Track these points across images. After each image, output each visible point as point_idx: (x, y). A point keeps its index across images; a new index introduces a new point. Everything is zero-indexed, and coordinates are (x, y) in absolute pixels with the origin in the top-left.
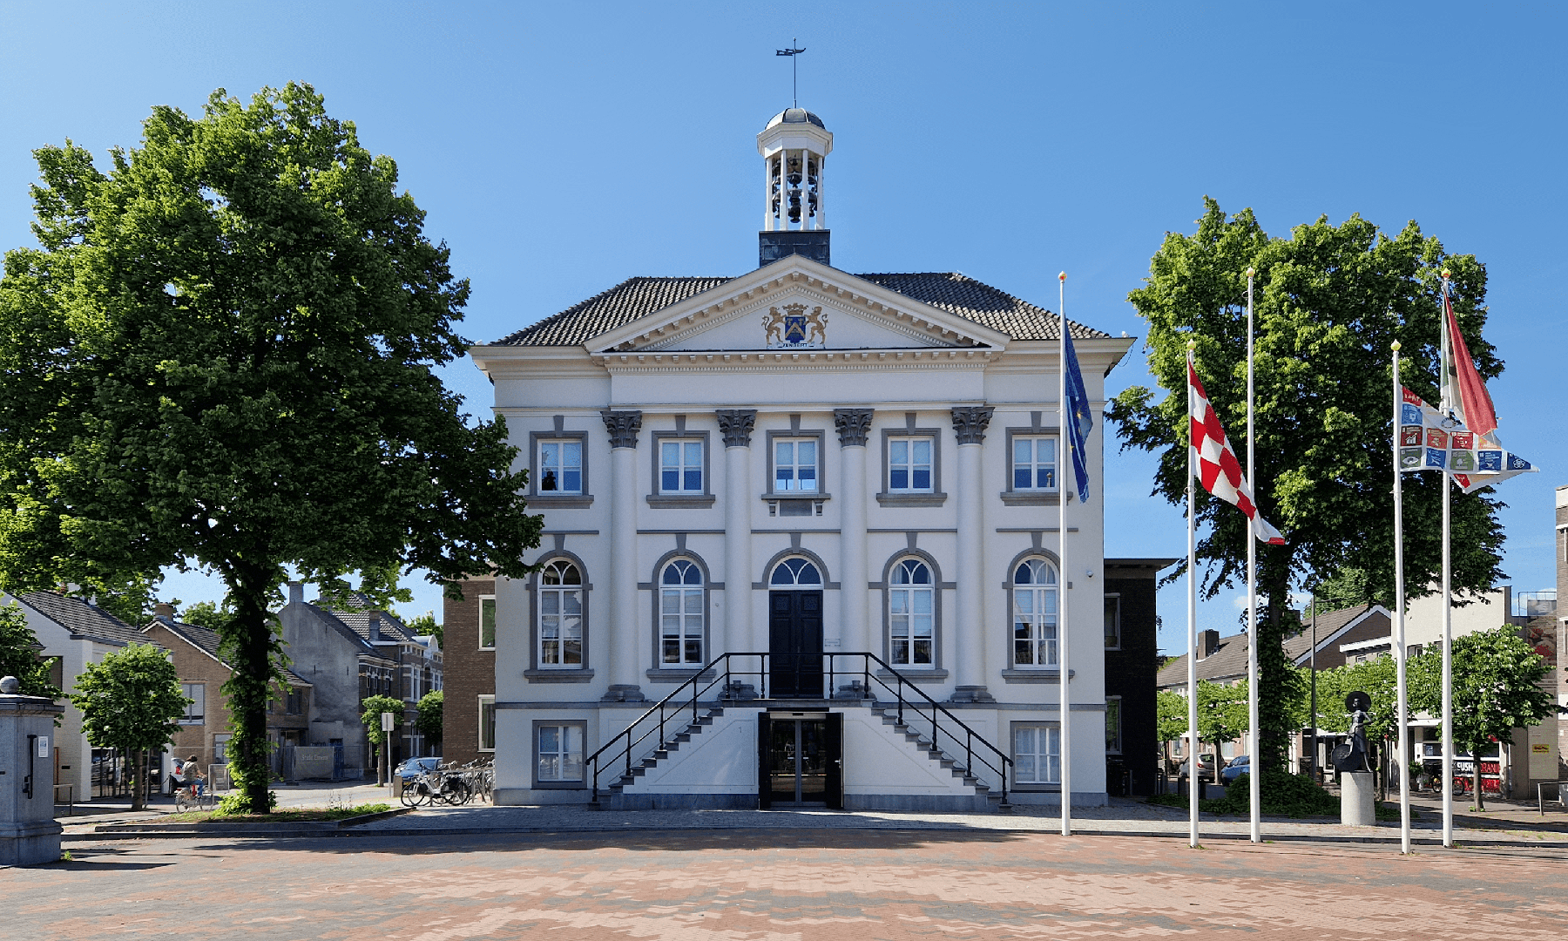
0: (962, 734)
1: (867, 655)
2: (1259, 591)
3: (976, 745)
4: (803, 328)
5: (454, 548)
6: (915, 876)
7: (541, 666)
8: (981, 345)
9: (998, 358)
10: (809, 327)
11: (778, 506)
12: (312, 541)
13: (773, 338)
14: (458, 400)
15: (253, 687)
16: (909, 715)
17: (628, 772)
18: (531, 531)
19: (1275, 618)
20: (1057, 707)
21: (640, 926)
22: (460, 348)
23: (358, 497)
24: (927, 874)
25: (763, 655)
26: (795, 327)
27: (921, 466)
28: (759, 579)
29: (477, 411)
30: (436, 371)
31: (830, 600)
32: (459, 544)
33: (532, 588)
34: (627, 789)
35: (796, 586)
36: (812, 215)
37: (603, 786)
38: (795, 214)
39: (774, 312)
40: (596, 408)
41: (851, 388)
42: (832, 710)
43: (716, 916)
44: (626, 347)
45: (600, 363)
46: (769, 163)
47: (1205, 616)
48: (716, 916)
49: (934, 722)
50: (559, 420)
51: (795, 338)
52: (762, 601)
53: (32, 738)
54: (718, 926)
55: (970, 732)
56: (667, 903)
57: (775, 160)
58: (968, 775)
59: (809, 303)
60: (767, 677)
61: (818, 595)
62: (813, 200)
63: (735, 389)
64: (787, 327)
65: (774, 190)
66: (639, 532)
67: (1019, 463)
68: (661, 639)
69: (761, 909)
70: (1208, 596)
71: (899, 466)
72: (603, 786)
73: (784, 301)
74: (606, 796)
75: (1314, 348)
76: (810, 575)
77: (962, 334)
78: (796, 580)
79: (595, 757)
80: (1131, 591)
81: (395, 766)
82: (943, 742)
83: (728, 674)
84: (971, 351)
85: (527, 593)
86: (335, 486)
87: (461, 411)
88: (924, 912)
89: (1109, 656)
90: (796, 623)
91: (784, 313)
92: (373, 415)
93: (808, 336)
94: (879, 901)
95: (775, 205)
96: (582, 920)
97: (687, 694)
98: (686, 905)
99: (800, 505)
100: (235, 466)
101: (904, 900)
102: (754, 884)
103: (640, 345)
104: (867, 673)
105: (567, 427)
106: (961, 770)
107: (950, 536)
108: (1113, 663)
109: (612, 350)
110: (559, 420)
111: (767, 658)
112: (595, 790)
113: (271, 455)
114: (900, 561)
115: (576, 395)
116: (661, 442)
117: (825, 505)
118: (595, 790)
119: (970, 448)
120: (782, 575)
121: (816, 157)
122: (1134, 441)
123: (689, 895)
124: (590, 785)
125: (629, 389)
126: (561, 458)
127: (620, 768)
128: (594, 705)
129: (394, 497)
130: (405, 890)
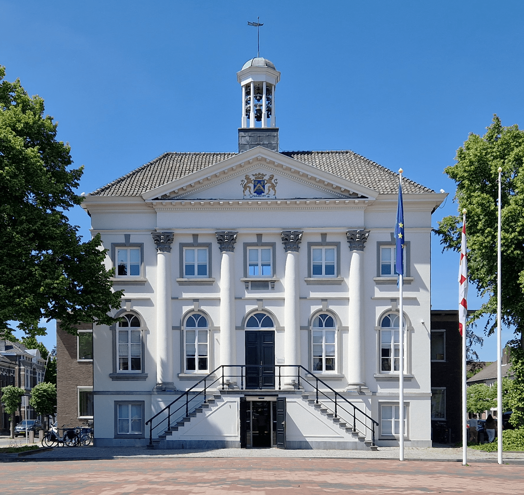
3: (358, 414)
4: (264, 187)
5: (74, 309)
6: (319, 475)
7: (118, 371)
8: (363, 197)
9: (371, 204)
10: (266, 186)
11: (250, 284)
13: (247, 192)
14: (76, 228)
17: (169, 429)
18: (115, 300)
21: (195, 489)
22: (78, 200)
23: (27, 284)
24: (324, 474)
25: (242, 366)
26: (259, 186)
27: (330, 263)
28: (239, 325)
29: (85, 236)
30: (65, 213)
32: (78, 307)
33: (113, 329)
34: (168, 438)
36: (268, 117)
37: (155, 436)
38: (258, 118)
39: (247, 178)
40: (148, 230)
41: (291, 220)
42: (280, 396)
43: (228, 486)
45: (151, 206)
46: (244, 89)
48: (228, 486)
49: (336, 402)
50: (127, 237)
51: (259, 192)
54: (229, 489)
55: (355, 408)
56: (205, 483)
57: (248, 86)
59: (267, 173)
60: (244, 378)
62: (269, 110)
63: (225, 220)
65: (247, 103)
66: (173, 298)
67: (384, 261)
68: (185, 357)
69: (249, 484)
71: (317, 262)
72: (155, 436)
73: (252, 172)
74: (157, 442)
76: (269, 322)
77: (352, 191)
78: (260, 325)
79: (151, 421)
81: (15, 425)
82: (340, 413)
83: (223, 376)
84: (357, 200)
85: (110, 333)
86: (15, 277)
88: (319, 486)
89: (433, 365)
90: (258, 350)
91: (253, 178)
92: (32, 240)
93: (266, 191)
94: (299, 483)
95: (248, 111)
96: (169, 488)
98: (213, 483)
101: (311, 483)
103: (172, 196)
105: (132, 240)
109: (157, 199)
110: (127, 237)
111: (244, 368)
112: (151, 438)
114: (318, 315)
115: (139, 225)
116: (184, 248)
118: (151, 438)
120: (252, 322)
122: (450, 246)
123: (214, 481)
124: (147, 435)
125: (167, 219)
126: (128, 257)
127: (164, 427)
128: (150, 393)
129: (47, 284)
130: (79, 479)
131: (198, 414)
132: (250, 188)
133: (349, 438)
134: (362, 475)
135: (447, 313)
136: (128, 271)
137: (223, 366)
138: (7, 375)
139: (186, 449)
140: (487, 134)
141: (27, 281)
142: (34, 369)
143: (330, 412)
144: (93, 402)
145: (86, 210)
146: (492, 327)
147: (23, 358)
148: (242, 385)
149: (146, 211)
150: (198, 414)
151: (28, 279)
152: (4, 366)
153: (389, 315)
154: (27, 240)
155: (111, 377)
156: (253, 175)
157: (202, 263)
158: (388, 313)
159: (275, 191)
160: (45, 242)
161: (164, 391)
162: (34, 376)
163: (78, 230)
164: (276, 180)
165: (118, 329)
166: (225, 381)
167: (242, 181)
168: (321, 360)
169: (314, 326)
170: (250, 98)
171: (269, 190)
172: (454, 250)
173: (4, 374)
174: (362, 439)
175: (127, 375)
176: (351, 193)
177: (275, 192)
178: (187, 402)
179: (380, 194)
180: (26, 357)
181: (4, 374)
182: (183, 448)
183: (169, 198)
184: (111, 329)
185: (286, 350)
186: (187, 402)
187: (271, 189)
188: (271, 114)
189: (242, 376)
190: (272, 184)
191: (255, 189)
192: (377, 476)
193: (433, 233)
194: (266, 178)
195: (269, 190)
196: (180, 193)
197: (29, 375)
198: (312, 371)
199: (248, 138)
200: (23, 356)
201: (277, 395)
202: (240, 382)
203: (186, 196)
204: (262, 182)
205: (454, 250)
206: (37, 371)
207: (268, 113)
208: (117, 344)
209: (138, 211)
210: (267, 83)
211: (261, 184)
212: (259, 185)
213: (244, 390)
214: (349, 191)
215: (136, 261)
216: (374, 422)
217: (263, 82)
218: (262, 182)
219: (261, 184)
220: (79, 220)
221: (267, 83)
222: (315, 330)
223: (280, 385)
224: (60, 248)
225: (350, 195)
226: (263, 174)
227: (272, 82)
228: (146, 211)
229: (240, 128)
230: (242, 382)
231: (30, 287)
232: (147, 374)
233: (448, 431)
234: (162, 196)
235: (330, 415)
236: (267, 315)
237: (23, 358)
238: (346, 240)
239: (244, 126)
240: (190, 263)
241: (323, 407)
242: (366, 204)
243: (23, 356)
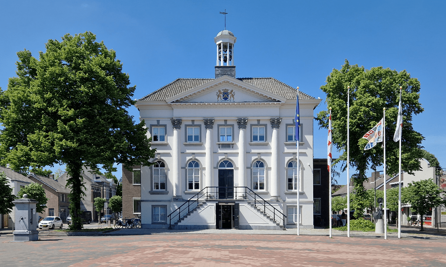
2: (358, 169)
4: (228, 96)
7: (154, 190)
8: (278, 101)
10: (229, 96)
12: (95, 157)
13: (219, 98)
14: (132, 117)
15: (77, 196)
18: (152, 154)
19: (361, 177)
20: (296, 203)
22: (133, 103)
23: (107, 145)
25: (217, 187)
26: (226, 95)
27: (262, 135)
28: (215, 166)
29: (137, 121)
32: (133, 157)
33: (151, 168)
36: (230, 60)
37: (172, 223)
38: (225, 61)
39: (219, 91)
40: (168, 118)
41: (242, 113)
44: (177, 101)
45: (170, 105)
46: (218, 46)
47: (343, 176)
50: (158, 121)
51: (226, 99)
53: (32, 209)
55: (275, 208)
57: (220, 45)
58: (274, 221)
59: (229, 89)
62: (231, 57)
63: (208, 113)
65: (220, 53)
70: (343, 171)
71: (255, 134)
73: (222, 88)
74: (173, 226)
75: (370, 104)
76: (230, 165)
79: (170, 215)
80: (320, 168)
81: (101, 217)
84: (275, 103)
85: (150, 170)
87: (133, 120)
90: (225, 179)
91: (222, 91)
92: (110, 123)
93: (229, 98)
95: (220, 58)
100: (75, 137)
101: (252, 247)
102: (217, 244)
103: (181, 100)
108: (315, 188)
109: (173, 102)
110: (158, 121)
113: (84, 133)
115: (164, 115)
116: (187, 127)
121: (232, 44)
122: (323, 126)
123: (202, 246)
125: (178, 113)
126: (159, 132)
127: (177, 218)
128: (170, 201)
132: (221, 96)
133: (271, 224)
136: (159, 139)
137: (207, 187)
150: (194, 212)
168: (257, 184)
169: (254, 167)
174: (278, 224)
185: (239, 179)
193: (314, 119)
194: (229, 91)
196: (185, 99)
198: (253, 190)
199: (220, 71)
206: (112, 190)
210: (229, 43)
216: (284, 216)
220: (134, 113)
221: (229, 43)
222: (254, 169)
227: (232, 42)
235: (262, 212)
236: (230, 161)
240: (191, 135)
241: (258, 208)
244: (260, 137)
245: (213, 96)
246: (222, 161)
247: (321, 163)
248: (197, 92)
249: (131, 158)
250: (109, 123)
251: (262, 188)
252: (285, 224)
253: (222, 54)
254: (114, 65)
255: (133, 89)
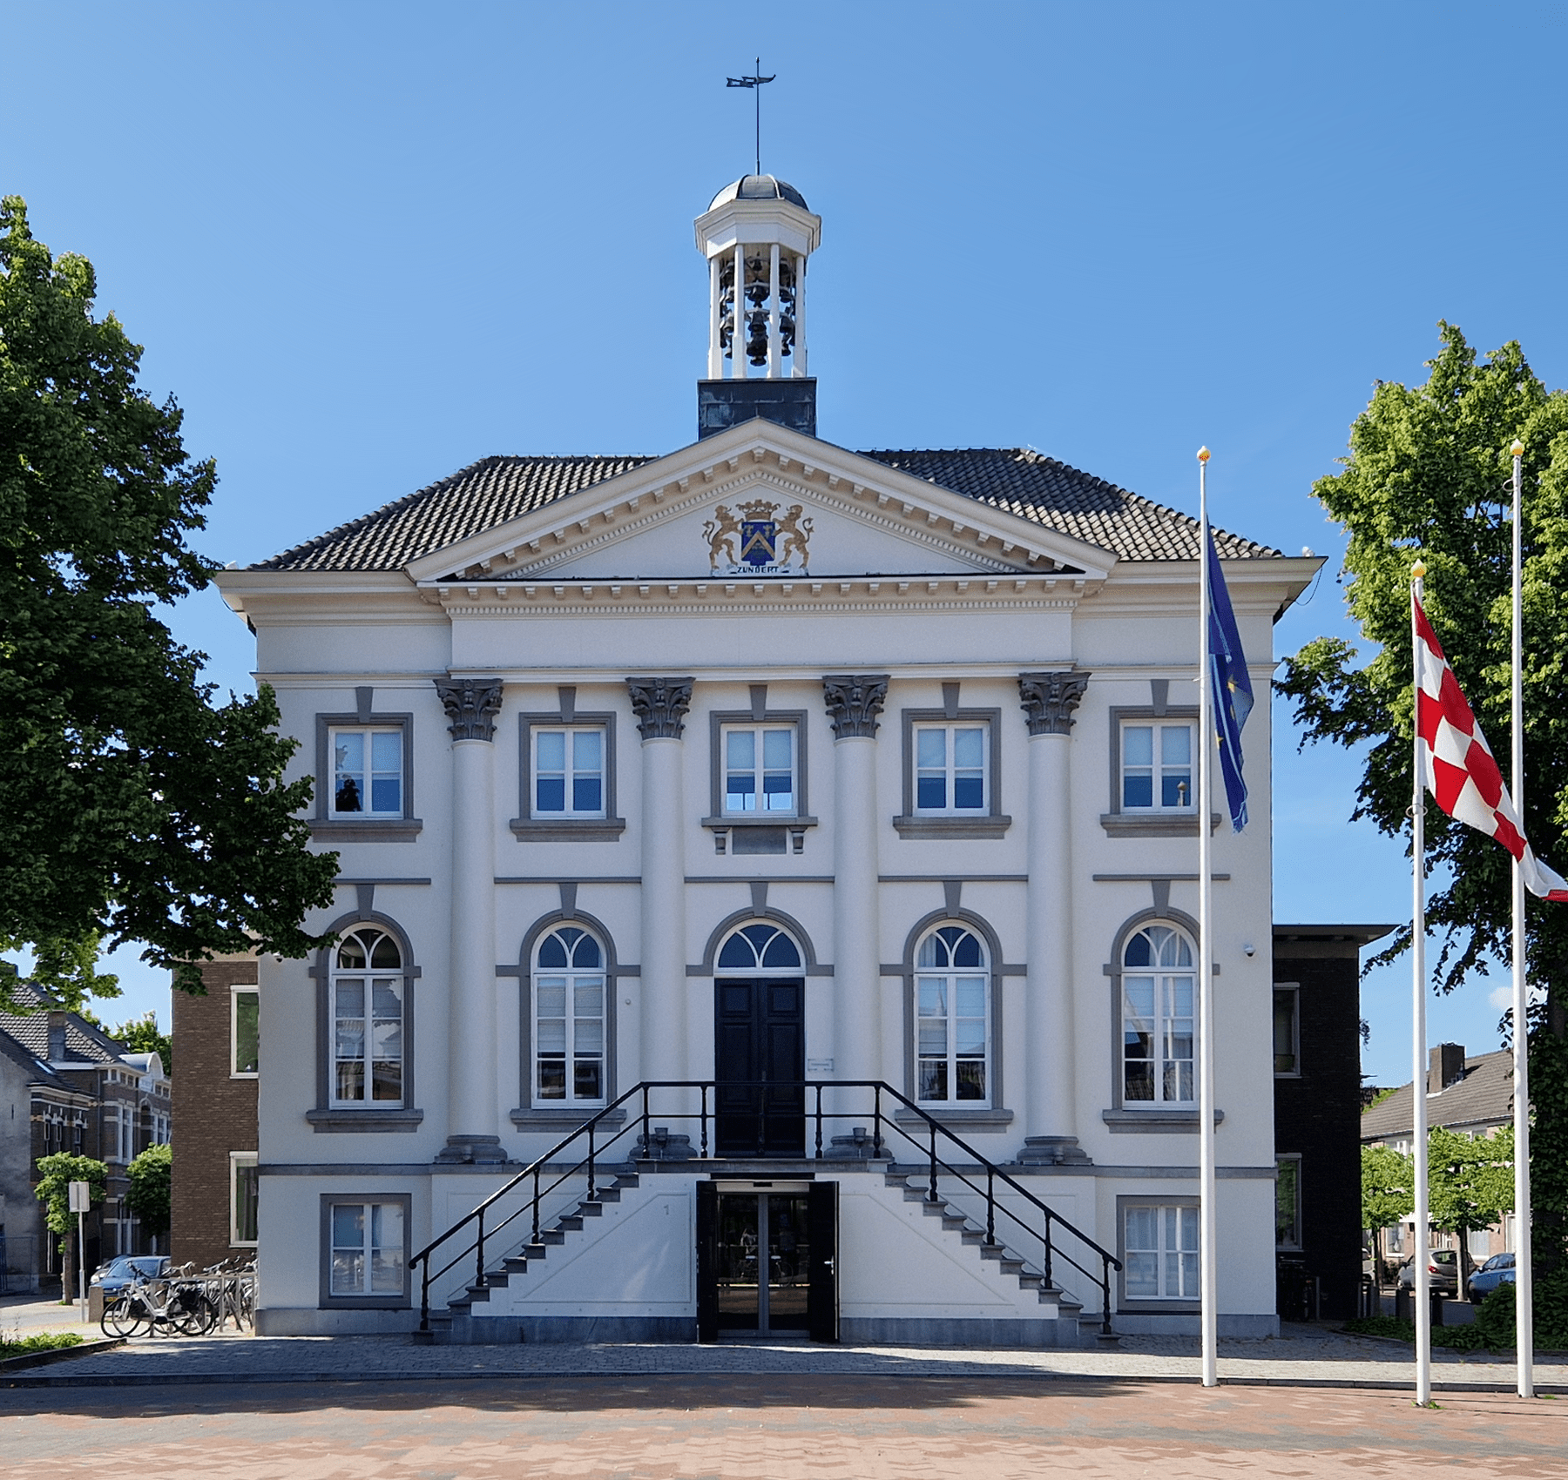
0: (1036, 1218)
1: (878, 1085)
2: (1531, 979)
3: (1059, 1234)
4: (771, 541)
5: (190, 908)
8: (1068, 570)
9: (1095, 590)
10: (780, 540)
11: (729, 837)
13: (722, 554)
16: (948, 1186)
17: (480, 1282)
18: (318, 879)
20: (1193, 1172)
22: (200, 574)
23: (31, 821)
25: (704, 1085)
28: (697, 959)
29: (227, 680)
30: (160, 612)
31: (816, 994)
32: (198, 900)
34: (478, 1309)
35: (759, 971)
36: (786, 353)
37: (438, 1302)
38: (757, 351)
39: (722, 515)
45: (432, 599)
49: (990, 1197)
50: (364, 695)
51: (758, 557)
52: (703, 994)
55: (1049, 1214)
57: (725, 261)
60: (711, 1122)
61: (797, 985)
62: (788, 328)
64: (745, 540)
67: (1131, 766)
68: (535, 1060)
70: (1447, 987)
71: (932, 770)
73: (738, 496)
74: (443, 1320)
76: (783, 953)
77: (1036, 552)
78: (759, 962)
79: (424, 1255)
80: (1317, 979)
81: (90, 1271)
82: (1005, 1230)
83: (646, 1117)
84: (1051, 579)
85: (310, 985)
87: (201, 679)
90: (760, 1033)
91: (739, 515)
92: (55, 685)
93: (779, 554)
97: (578, 1150)
99: (765, 835)
103: (499, 569)
104: (877, 1116)
105: (379, 706)
106: (1036, 1278)
107: (629, 891)
109: (452, 578)
110: (364, 695)
111: (711, 1091)
112: (425, 1310)
114: (932, 929)
115: (389, 651)
116: (534, 730)
117: (809, 835)
118: (425, 1310)
119: (1050, 742)
120: (736, 953)
122: (1322, 730)
125: (482, 642)
126: (367, 758)
127: (466, 1274)
131: (569, 1235)
132: (730, 544)
134: (1107, 1451)
135: (1313, 933)
136: (367, 798)
138: (66, 1123)
139: (532, 1342)
140: (1430, 382)
141: (29, 814)
142: (146, 1108)
143: (972, 1227)
144: (256, 1198)
145: (244, 616)
146: (1457, 966)
147: (114, 1077)
148: (704, 1144)
149: (415, 616)
150: (569, 1235)
151: (34, 809)
152: (55, 1099)
153: (1147, 931)
154: (37, 685)
155: (310, 1121)
156: (741, 507)
157: (587, 771)
158: (1145, 925)
159: (806, 554)
160: (94, 690)
161: (471, 1162)
162: (146, 1127)
163: (202, 667)
164: (810, 520)
165: (335, 972)
166: (651, 1131)
167: (707, 524)
168: (942, 1068)
169: (923, 964)
170: (732, 293)
171: (788, 552)
172: (1335, 740)
173: (55, 1121)
174: (1068, 1308)
175: (359, 1115)
176: (1033, 557)
177: (806, 558)
178: (537, 1197)
179: (1120, 561)
180: (123, 1075)
181: (55, 1121)
182: (522, 1340)
183: (490, 576)
184: (312, 972)
186: (537, 1197)
187: (792, 547)
188: (793, 343)
189: (704, 1116)
190: (797, 533)
191: (747, 549)
192: (1161, 1455)
193: (1274, 692)
194: (779, 515)
195: (788, 552)
196: (521, 561)
197: (131, 1125)
198: (917, 1103)
200: (114, 1072)
201: (812, 1176)
202: (699, 1134)
203: (540, 570)
204: (767, 528)
205: (1335, 740)
206: (155, 1113)
207: (784, 341)
208: (332, 1019)
209: (396, 616)
210: (782, 248)
211: (763, 532)
212: (757, 536)
213: (711, 1157)
214: (1027, 552)
215: (391, 767)
216: (1107, 1258)
217: (770, 245)
218: (767, 528)
219: (763, 532)
220: (217, 643)
221: (782, 248)
222: (925, 972)
223: (819, 1143)
224: (142, 713)
225: (1031, 563)
226: (768, 505)
227: (798, 246)
228: (415, 616)
229: (702, 378)
230: (704, 1136)
231: (37, 832)
232: (421, 1111)
233: (1313, 1285)
234: (467, 570)
236: (782, 929)
237: (114, 1077)
238: (1018, 701)
239: (714, 373)
240: (551, 772)
242: (1079, 591)
243: (114, 1072)
244: (959, 783)
245: (681, 545)
246: (737, 929)
247: (1314, 953)
248: (591, 519)
249: (190, 908)
250: (46, 684)
251: (969, 1090)
252: (1113, 1310)
253: (735, 309)
254: (68, 318)
255: (204, 484)
